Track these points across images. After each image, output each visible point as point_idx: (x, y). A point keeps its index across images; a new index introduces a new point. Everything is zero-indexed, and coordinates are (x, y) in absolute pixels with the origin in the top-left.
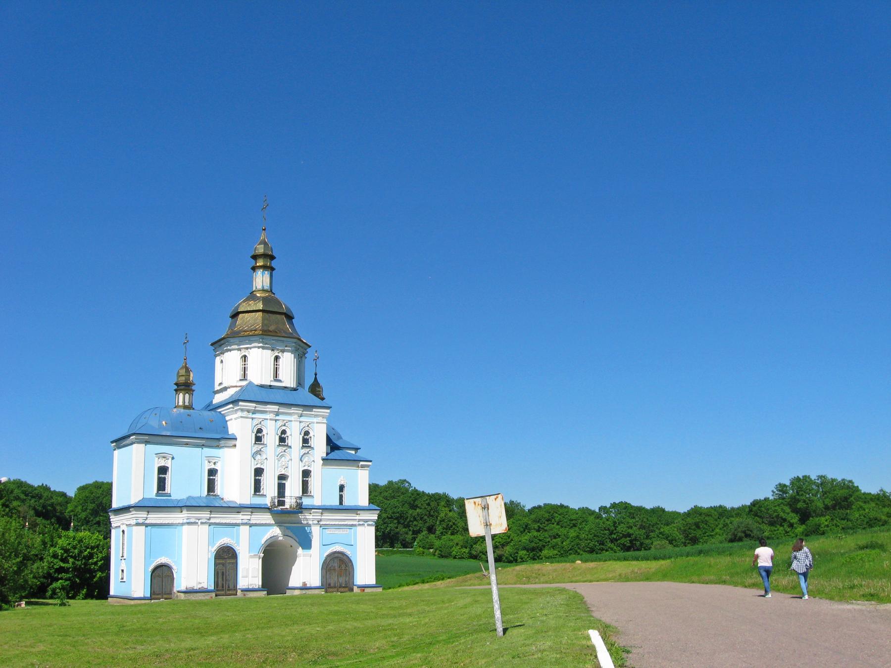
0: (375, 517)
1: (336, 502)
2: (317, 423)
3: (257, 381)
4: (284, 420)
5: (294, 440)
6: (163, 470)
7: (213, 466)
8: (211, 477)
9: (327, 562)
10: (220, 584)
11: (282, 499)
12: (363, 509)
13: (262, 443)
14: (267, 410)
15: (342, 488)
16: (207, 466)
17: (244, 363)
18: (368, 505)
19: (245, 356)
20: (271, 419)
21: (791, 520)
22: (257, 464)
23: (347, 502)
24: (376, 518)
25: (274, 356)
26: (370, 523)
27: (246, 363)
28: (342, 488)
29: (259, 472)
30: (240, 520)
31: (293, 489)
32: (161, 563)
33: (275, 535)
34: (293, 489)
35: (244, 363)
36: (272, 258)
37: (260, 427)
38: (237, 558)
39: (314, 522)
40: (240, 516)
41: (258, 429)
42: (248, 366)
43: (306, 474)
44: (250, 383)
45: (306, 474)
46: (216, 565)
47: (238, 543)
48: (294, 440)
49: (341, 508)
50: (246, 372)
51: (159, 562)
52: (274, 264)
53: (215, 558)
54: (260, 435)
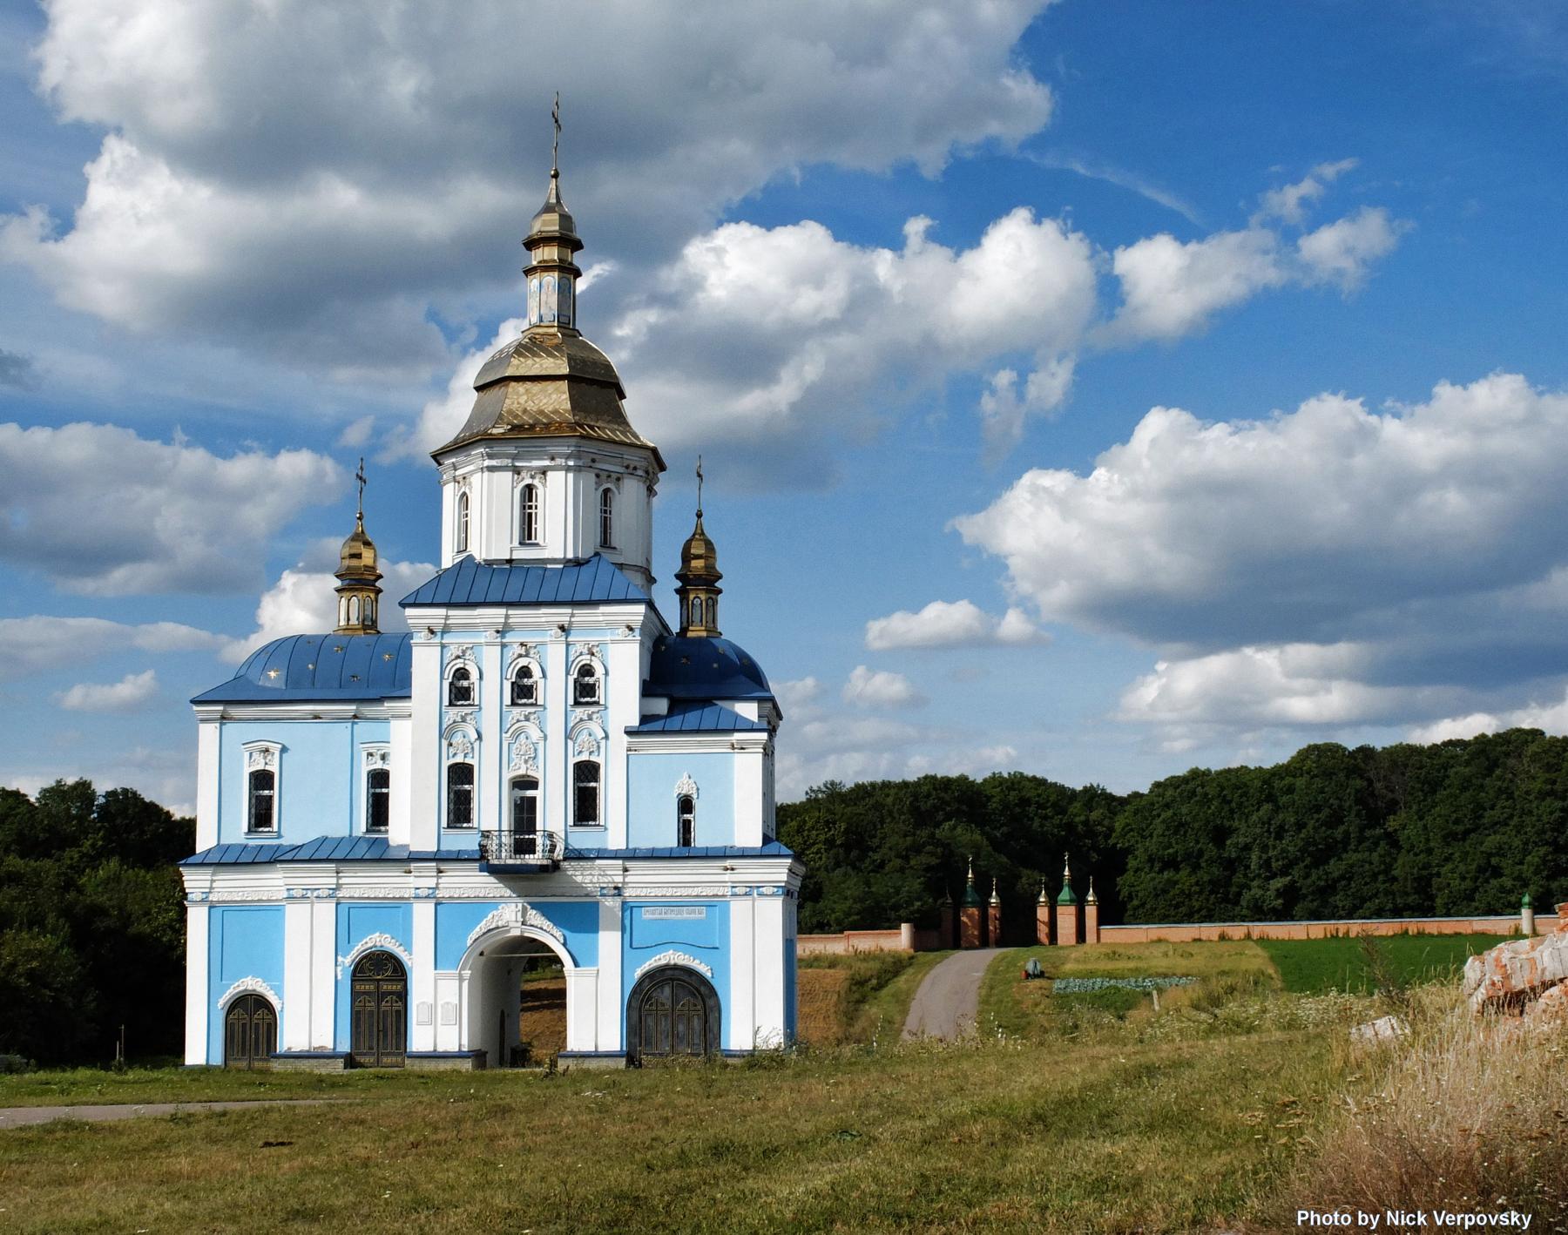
0: (782, 876)
1: (670, 840)
2: (613, 642)
3: (479, 551)
4: (461, 644)
5: (554, 689)
6: (262, 780)
7: (379, 765)
8: (378, 791)
9: (641, 991)
10: (730, 1061)
11: (531, 837)
12: (744, 854)
13: (471, 702)
14: (478, 621)
15: (686, 805)
16: (365, 767)
17: (533, 511)
18: (760, 845)
19: (529, 489)
20: (488, 644)
21: (143, 832)
22: (581, 752)
23: (701, 839)
24: (784, 877)
25: (601, 489)
26: (769, 890)
27: (533, 504)
28: (686, 805)
29: (461, 775)
30: (413, 891)
31: (554, 812)
32: (246, 990)
33: (500, 924)
34: (554, 812)
35: (533, 511)
36: (577, 246)
37: (462, 666)
38: (716, 995)
39: (736, 890)
40: (411, 879)
41: (583, 666)
42: (540, 511)
43: (586, 772)
44: (470, 557)
45: (586, 772)
46: (355, 995)
47: (408, 946)
48: (554, 689)
49: (685, 849)
50: (534, 526)
51: (241, 988)
52: (577, 259)
53: (352, 981)
54: (465, 683)
